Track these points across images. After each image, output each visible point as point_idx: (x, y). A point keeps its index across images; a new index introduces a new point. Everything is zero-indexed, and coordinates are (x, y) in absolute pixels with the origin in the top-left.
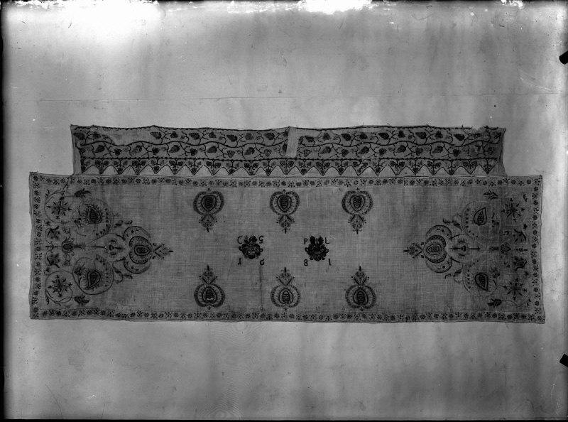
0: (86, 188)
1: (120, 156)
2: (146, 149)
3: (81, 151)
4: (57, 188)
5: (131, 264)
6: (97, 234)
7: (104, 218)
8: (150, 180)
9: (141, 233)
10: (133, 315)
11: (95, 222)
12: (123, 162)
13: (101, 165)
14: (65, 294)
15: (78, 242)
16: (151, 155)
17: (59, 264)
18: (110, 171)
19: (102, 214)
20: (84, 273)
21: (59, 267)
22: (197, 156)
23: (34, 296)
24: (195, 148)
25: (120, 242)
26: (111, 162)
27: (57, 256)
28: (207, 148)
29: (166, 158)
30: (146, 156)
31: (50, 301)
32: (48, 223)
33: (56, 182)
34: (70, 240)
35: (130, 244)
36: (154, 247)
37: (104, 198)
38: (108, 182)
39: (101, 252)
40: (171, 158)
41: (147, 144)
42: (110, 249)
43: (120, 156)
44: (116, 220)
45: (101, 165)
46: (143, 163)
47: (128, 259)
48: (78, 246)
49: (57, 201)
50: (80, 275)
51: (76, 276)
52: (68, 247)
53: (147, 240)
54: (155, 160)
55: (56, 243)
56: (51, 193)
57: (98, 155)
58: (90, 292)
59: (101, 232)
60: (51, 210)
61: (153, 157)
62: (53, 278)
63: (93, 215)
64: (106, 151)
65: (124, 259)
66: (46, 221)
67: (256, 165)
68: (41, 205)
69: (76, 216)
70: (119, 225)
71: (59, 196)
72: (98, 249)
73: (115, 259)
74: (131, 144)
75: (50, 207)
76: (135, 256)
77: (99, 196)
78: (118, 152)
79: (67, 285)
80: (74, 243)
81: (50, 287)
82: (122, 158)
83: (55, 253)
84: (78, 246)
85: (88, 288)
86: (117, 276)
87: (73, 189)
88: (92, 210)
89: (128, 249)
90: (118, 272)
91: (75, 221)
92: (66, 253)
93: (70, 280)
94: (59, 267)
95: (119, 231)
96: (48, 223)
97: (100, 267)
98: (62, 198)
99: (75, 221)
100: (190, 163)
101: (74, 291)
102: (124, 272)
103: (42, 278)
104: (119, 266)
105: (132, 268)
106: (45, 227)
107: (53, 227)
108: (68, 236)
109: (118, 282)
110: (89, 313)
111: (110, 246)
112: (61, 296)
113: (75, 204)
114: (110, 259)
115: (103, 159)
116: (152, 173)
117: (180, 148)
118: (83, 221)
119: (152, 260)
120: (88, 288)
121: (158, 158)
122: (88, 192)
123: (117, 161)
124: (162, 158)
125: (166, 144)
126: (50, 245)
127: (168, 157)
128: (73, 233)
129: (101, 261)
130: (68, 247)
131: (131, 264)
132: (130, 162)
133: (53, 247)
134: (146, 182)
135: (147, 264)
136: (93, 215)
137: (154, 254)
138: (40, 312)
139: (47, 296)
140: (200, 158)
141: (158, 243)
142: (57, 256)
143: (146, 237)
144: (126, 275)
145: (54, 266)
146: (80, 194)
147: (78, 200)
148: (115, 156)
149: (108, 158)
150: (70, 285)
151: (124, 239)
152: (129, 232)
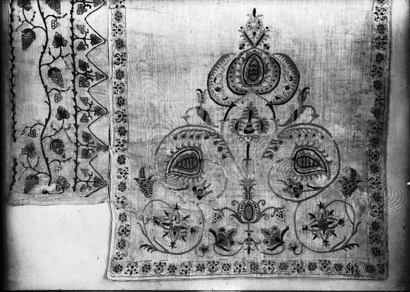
0: (133, 175)
1: (71, 111)
2: (54, 59)
3: (62, 186)
4: (135, 231)
5: (280, 91)
6: (224, 157)
7: (192, 143)
8: (116, 52)
9: (222, 71)
10: (378, 85)
11: (201, 161)
12: (81, 105)
13: (90, 147)
14: (339, 213)
15: (240, 192)
16: (66, 50)
17: (282, 229)
18: (101, 129)
19: (184, 147)
20: (297, 179)
21: (287, 229)
22: (66, 34)
23: (344, 271)
24: (55, 112)
25: (237, 113)
26: (83, 128)
27: (266, 232)
28: (54, 86)
29: (72, 20)
30: (69, 60)
31: (352, 242)
32: (205, 250)
33: (125, 231)
34: (235, 208)
35: (242, 93)
36: (246, 48)
37: (152, 142)
38: (122, 132)
39: (257, 150)
40: (72, 12)
41: (46, 55)
42: (252, 131)
43: (71, 111)
44: (196, 119)
45: (90, 147)
46: (83, 66)
47: (270, 97)
48: (248, 193)
49: (160, 230)
50: (301, 187)
51: (304, 195)
52: (248, 212)
53: (234, 62)
54: (77, 42)
55: (241, 236)
56: (146, 242)
57: (70, 152)
58: (334, 169)
59: (220, 149)
60: (179, 242)
61: (72, 47)
62: (308, 239)
63: (188, 164)
64: (63, 137)
65: (270, 105)
66: (200, 253)
67: (87, 137)
68: (171, 260)
69: (189, 196)
70: (205, 115)
71: (150, 226)
72: (251, 155)
73: (271, 122)
74: (46, 87)
75: (173, 244)
76: (265, 84)
77: (147, 152)
78: (62, 114)
79: (322, 211)
80: (240, 200)
81: (326, 242)
82: (76, 107)
83: (261, 237)
84: (248, 193)
85: (327, 171)
86: (305, 117)
87: (136, 199)
88: (176, 166)
89: (251, 97)
90: (296, 115)
91: (200, 198)
92: (261, 214)
93: (312, 205)
94: (287, 229)
95: (217, 115)
96: (205, 250)
97: (285, 151)
98: (156, 221)
99: (200, 198)
100: (85, 119)
101: (333, 198)
102: (295, 103)
103: (308, 257)
104: (284, 113)
105: (287, 88)
106: (213, 255)
107: (213, 240)
108: (227, 213)
109: (315, 116)
110: (375, 169)
111: (246, 132)
112: (341, 222)
113: (165, 195)
114: (271, 132)
115: (77, 144)
116: (104, 119)
117: (53, 65)
118: (199, 184)
119: (272, 51)
120: (327, 171)
121: (73, 38)
122: (142, 172)
123: (80, 116)
124: (72, 29)
125: (44, 19)
126: (246, 246)
127: (69, 16)
128: (222, 202)
129: (276, 149)
130: (248, 212)
131: (280, 91)
132: (83, 163)
133: (249, 240)
134: (121, 59)
135: (281, 60)
136: (188, 164)
137: (261, 47)
138: (374, 262)
139: (343, 248)
140: (74, 100)
141: (239, 39)
142: (266, 232)
143: (228, 61)
144: (303, 97)
145: (285, 238)
146: (146, 186)
147: (160, 192)
148: (71, 120)
149: (76, 135)
150: (321, 206)
151: (233, 105)
152: (220, 95)
